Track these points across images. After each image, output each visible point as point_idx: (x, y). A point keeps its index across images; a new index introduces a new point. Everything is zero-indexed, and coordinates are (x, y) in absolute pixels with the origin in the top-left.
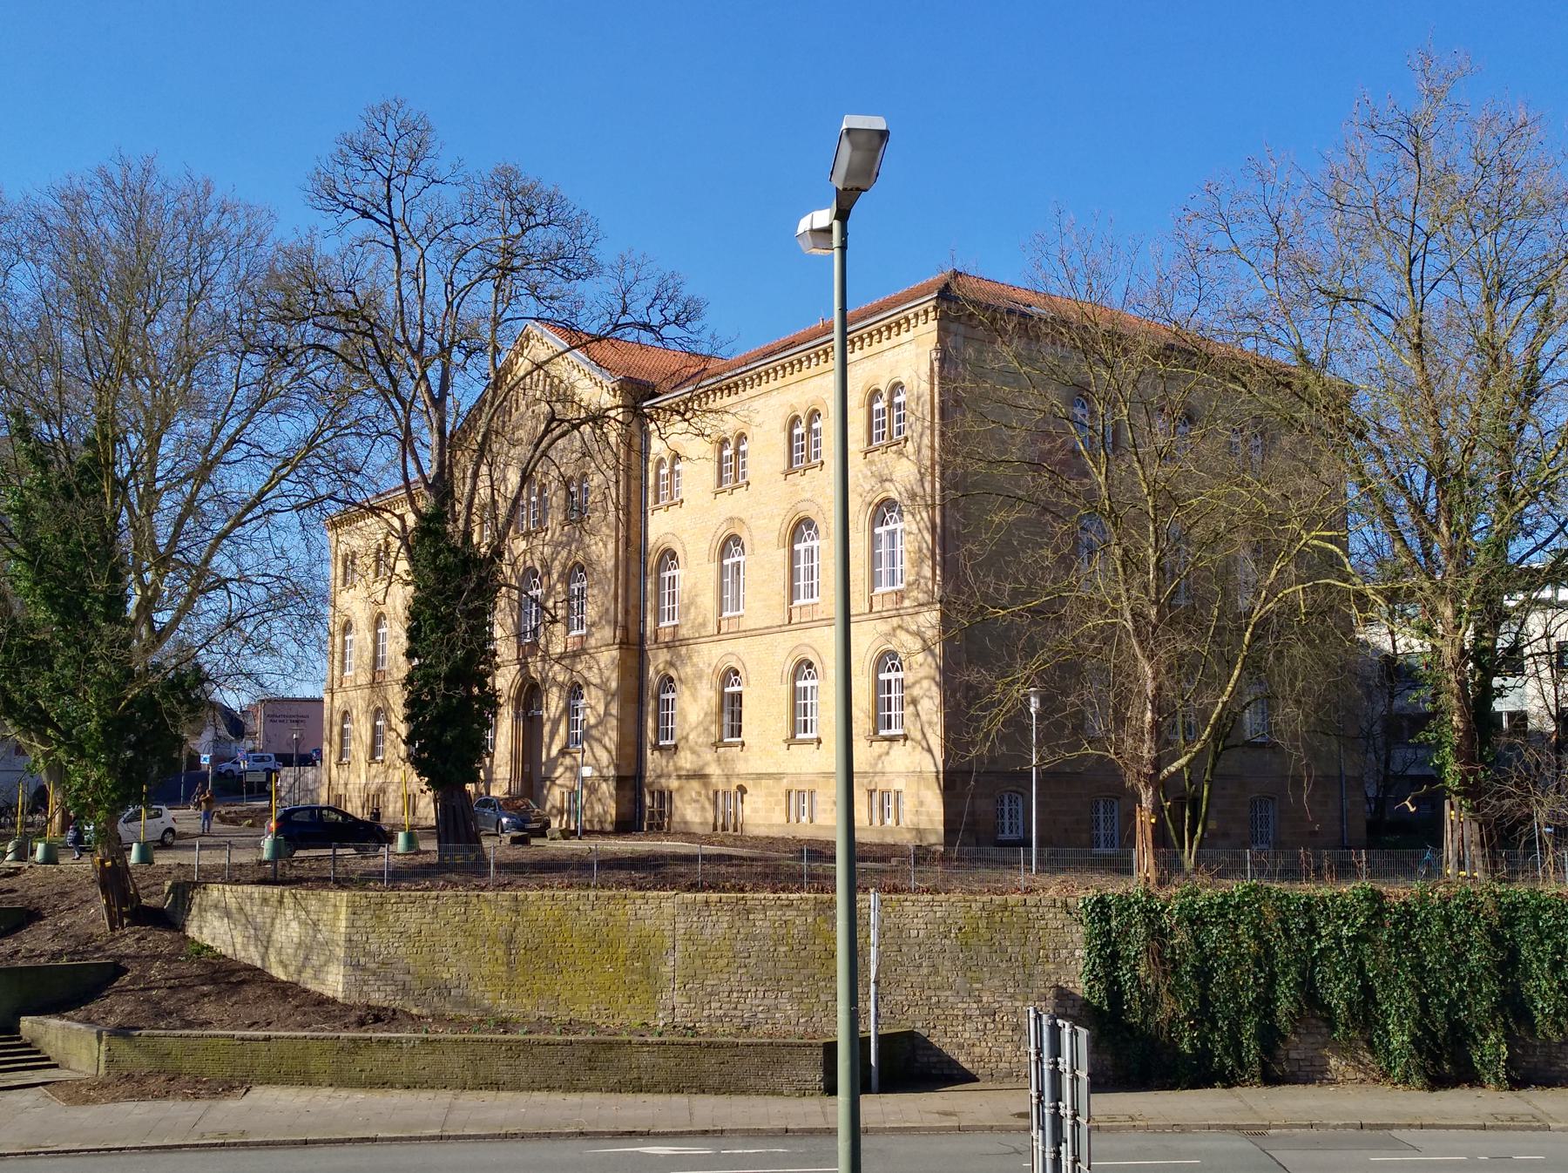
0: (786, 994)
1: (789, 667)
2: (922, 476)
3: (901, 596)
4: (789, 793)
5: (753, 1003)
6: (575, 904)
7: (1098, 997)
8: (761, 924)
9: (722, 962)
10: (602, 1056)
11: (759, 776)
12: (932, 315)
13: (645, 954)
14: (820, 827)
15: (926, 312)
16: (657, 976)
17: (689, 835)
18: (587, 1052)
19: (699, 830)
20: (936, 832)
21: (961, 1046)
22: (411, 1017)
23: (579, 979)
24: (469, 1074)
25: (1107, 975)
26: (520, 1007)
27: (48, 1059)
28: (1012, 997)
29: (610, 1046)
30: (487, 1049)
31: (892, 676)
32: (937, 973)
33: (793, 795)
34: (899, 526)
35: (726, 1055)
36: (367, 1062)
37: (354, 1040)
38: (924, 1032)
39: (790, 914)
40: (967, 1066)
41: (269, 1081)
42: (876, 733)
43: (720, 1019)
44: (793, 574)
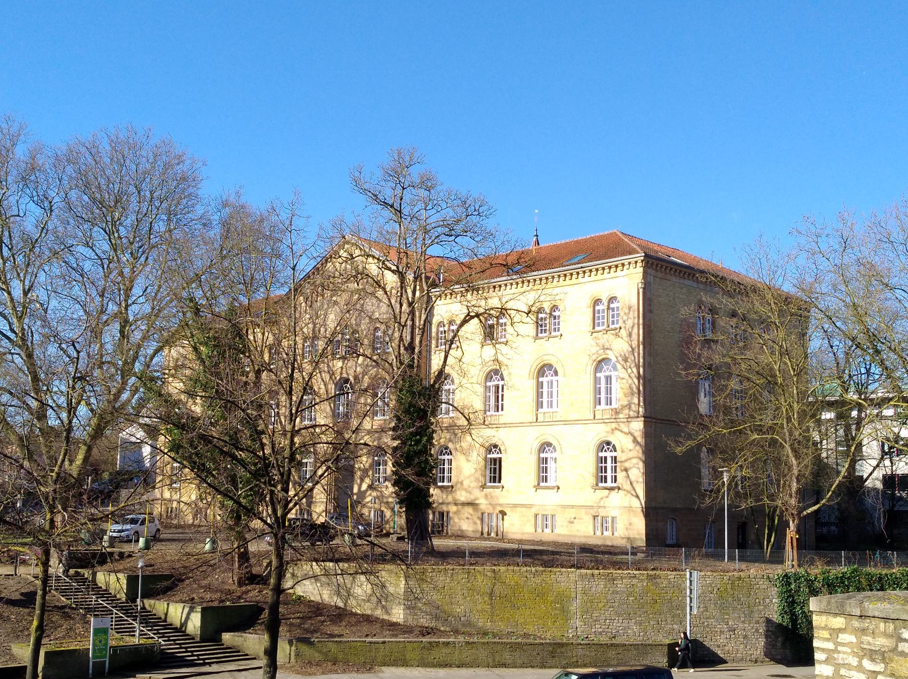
0: (633, 621)
1: (536, 445)
2: (633, 350)
3: (617, 412)
4: (536, 516)
5: (618, 625)
6: (525, 574)
7: (786, 621)
8: (621, 585)
9: (601, 605)
10: (558, 650)
11: (515, 506)
12: (639, 264)
13: (563, 600)
14: (559, 535)
15: (636, 262)
16: (568, 611)
17: (461, 536)
18: (551, 649)
19: (471, 534)
20: (641, 539)
21: (719, 646)
22: (440, 631)
23: (528, 612)
24: (490, 660)
25: (791, 611)
26: (501, 626)
27: (247, 655)
28: (743, 622)
29: (562, 645)
30: (499, 647)
31: (609, 454)
32: (707, 611)
33: (540, 517)
34: (614, 374)
35: (620, 650)
36: (440, 654)
37: (430, 643)
38: (701, 640)
39: (635, 581)
40: (722, 656)
41: (385, 664)
42: (597, 485)
43: (600, 633)
44: (539, 395)
